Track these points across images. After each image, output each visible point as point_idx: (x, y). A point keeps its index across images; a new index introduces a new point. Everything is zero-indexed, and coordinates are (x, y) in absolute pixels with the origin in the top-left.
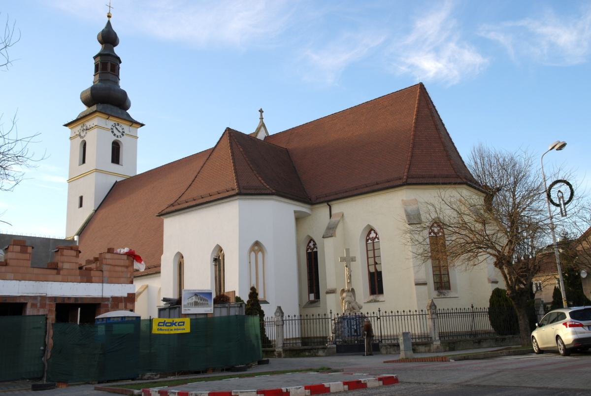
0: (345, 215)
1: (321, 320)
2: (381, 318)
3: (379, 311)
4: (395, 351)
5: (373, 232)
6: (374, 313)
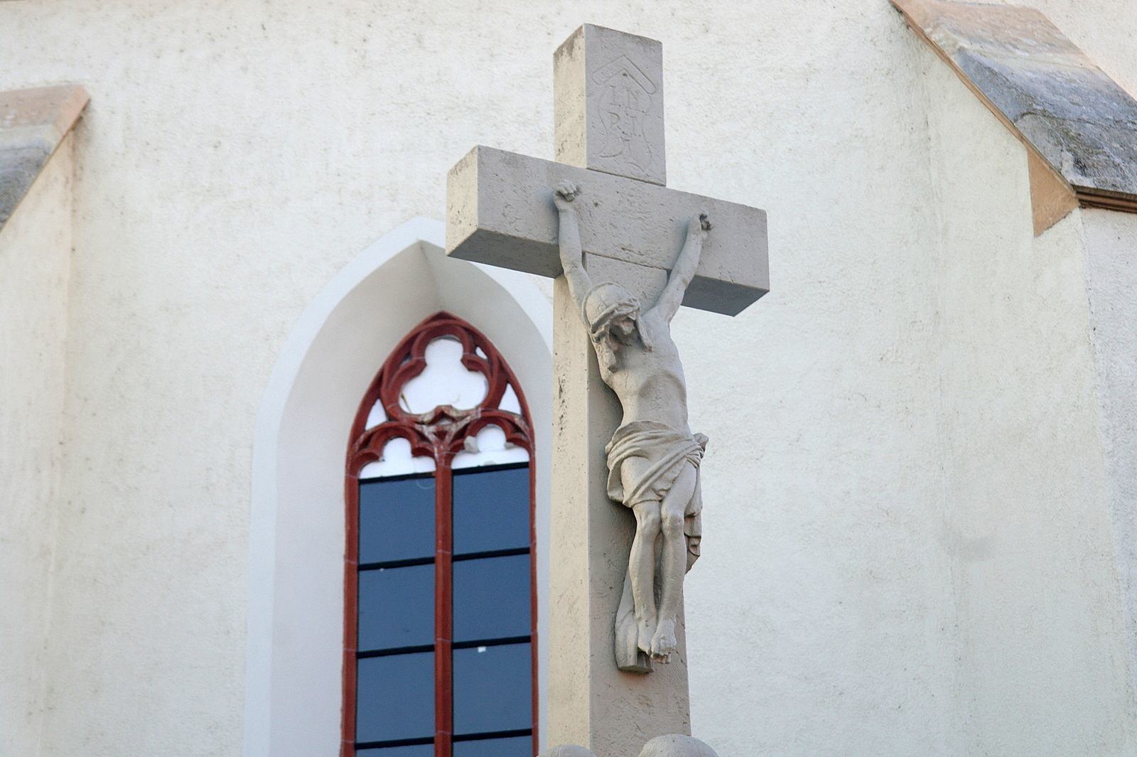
0: (100, 118)
5: (444, 354)
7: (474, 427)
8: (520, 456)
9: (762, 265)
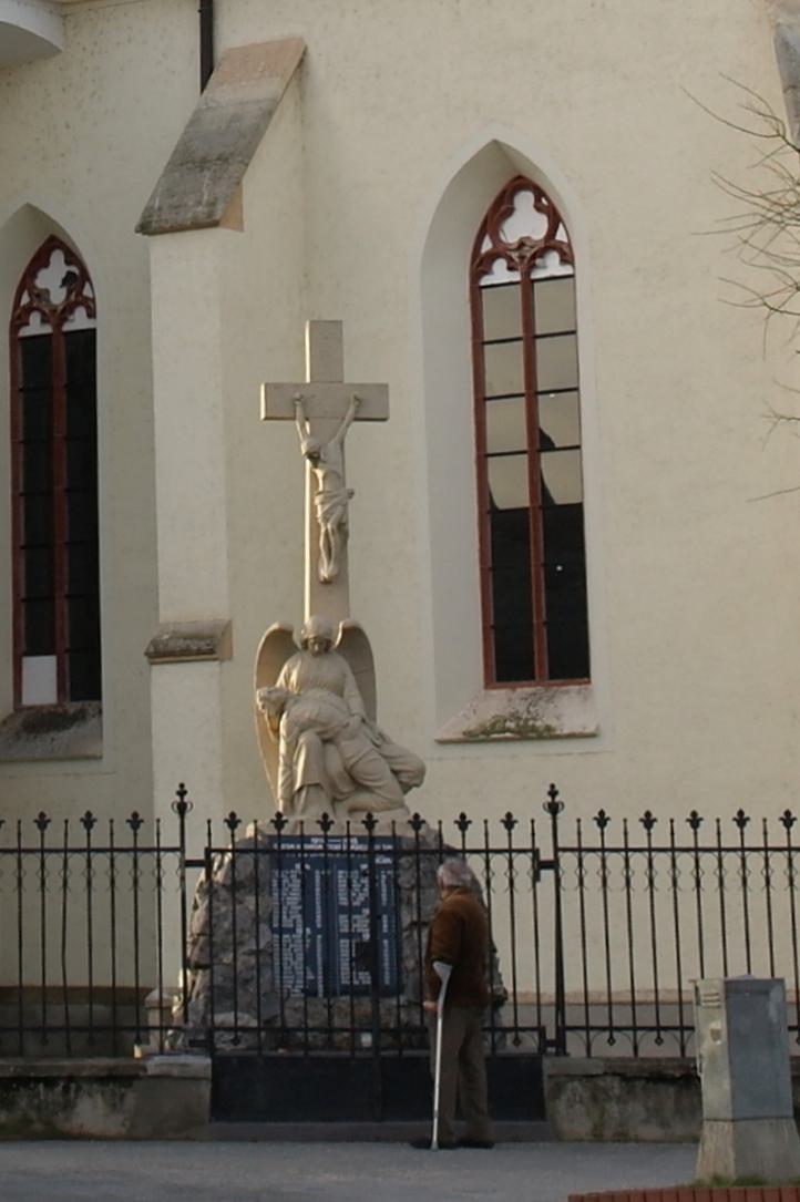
0: (316, 62)
1: (54, 861)
2: (568, 861)
3: (554, 809)
4: (664, 1124)
5: (525, 200)
6: (509, 822)
7: (541, 252)
8: (567, 270)
9: (386, 407)
